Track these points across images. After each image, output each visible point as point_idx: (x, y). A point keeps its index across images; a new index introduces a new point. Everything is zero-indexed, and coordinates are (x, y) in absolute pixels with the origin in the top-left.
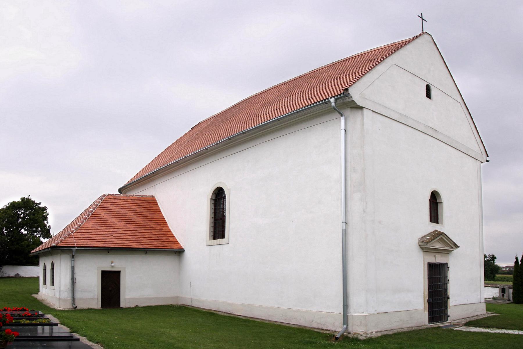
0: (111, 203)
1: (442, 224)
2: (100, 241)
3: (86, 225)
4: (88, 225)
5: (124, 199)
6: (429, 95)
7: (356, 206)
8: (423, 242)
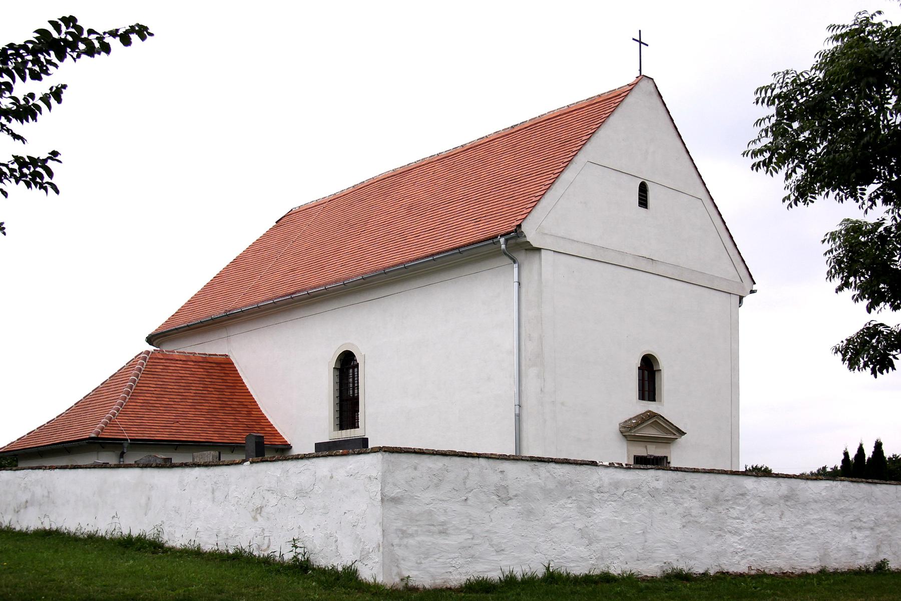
0: (161, 367)
1: (661, 401)
2: (162, 430)
3: (131, 404)
4: (134, 404)
5: (181, 360)
6: (643, 202)
7: (531, 385)
8: (625, 427)
